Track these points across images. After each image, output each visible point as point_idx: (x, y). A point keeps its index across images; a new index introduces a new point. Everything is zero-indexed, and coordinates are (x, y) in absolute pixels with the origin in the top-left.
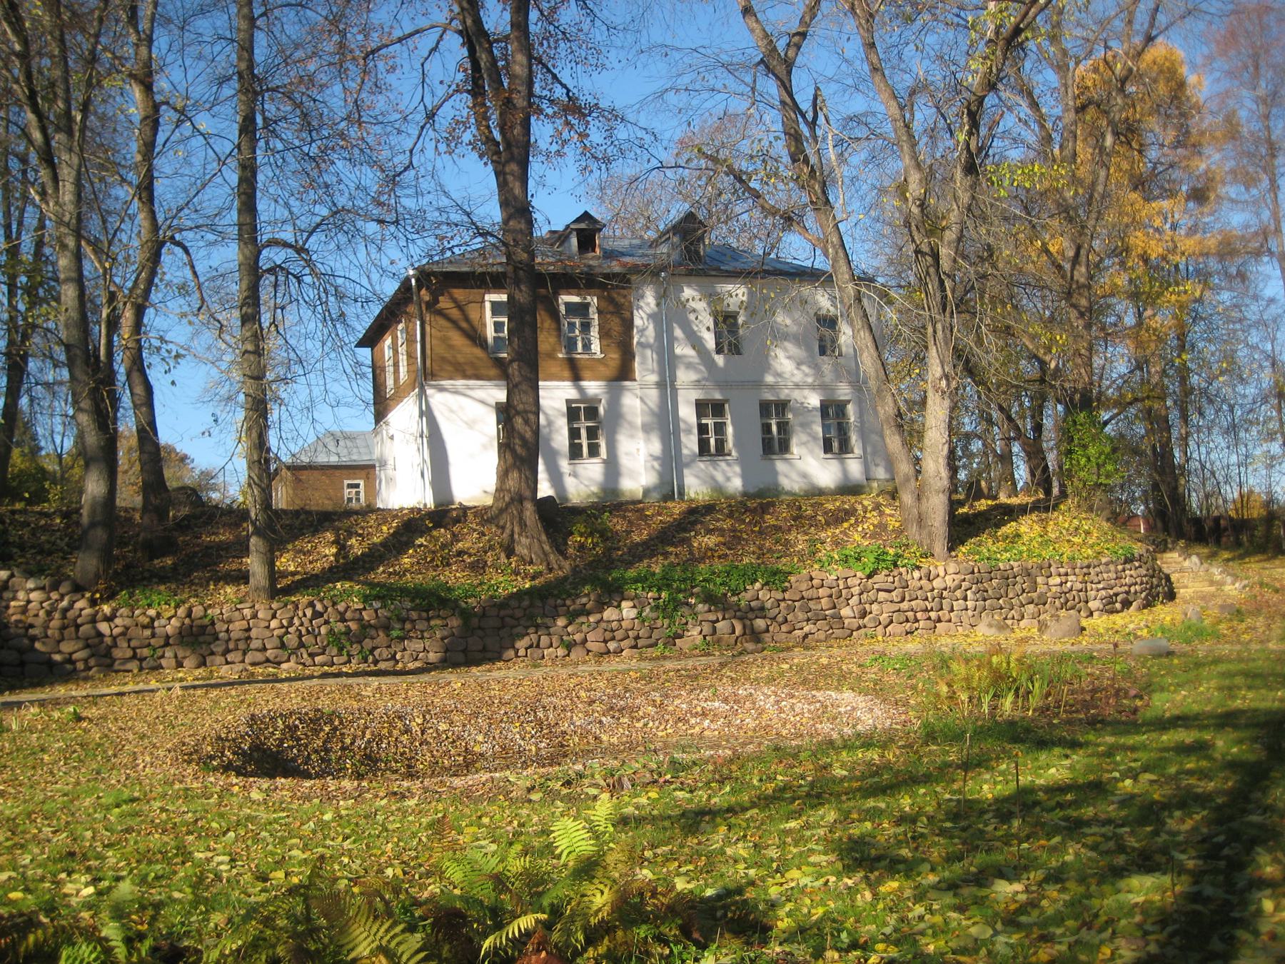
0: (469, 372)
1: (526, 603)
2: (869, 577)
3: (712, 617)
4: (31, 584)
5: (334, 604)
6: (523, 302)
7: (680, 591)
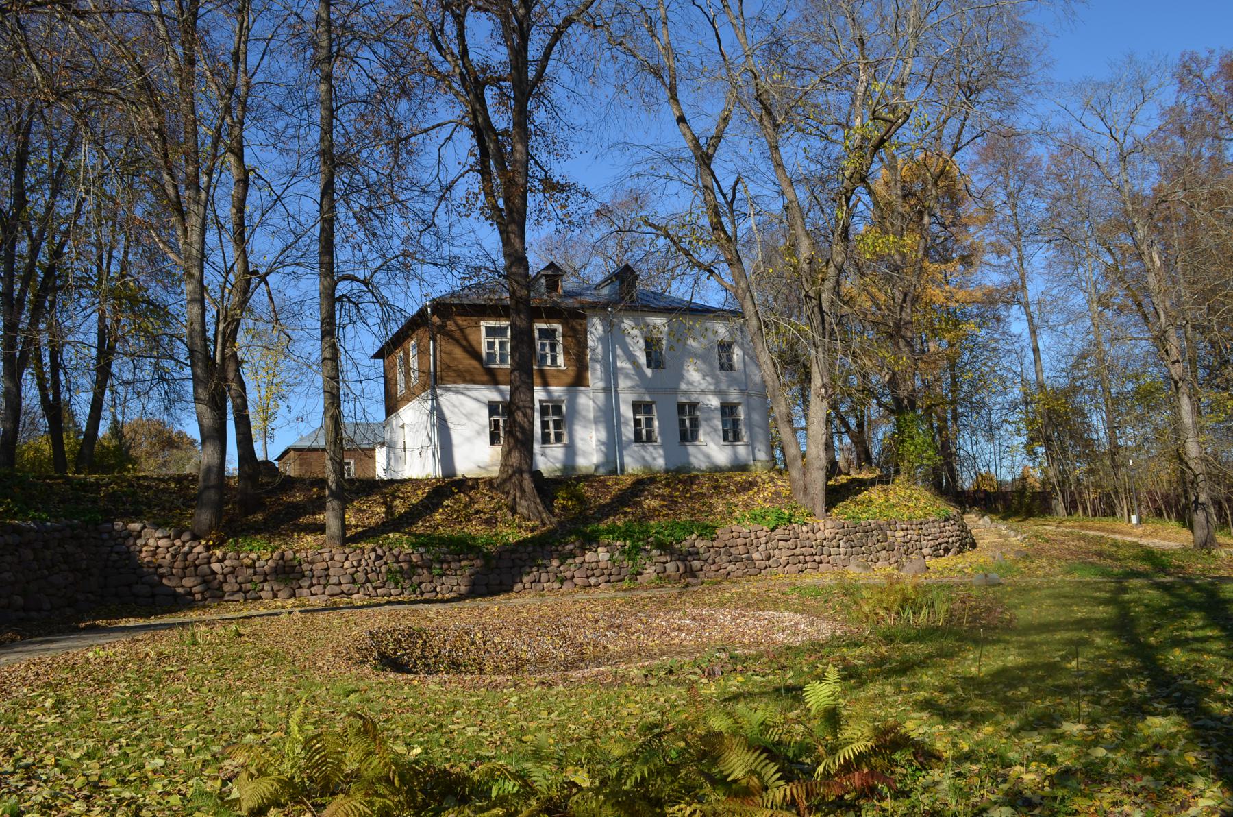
0: (468, 378)
1: (530, 549)
2: (772, 530)
3: (663, 559)
4: (159, 534)
5: (391, 549)
6: (518, 325)
7: (639, 540)
